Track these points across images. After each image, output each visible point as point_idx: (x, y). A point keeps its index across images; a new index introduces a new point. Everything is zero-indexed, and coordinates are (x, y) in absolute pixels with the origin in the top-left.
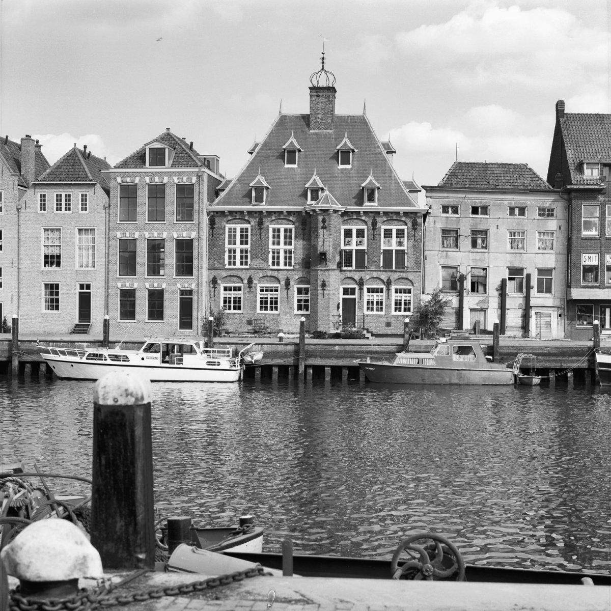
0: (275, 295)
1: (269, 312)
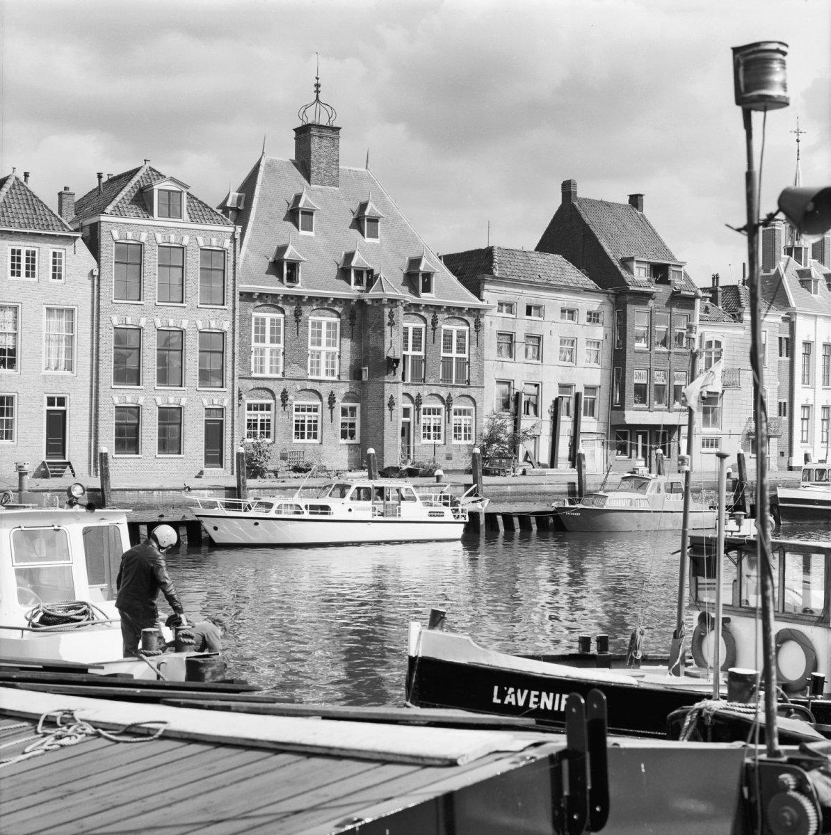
0: (254, 415)
1: (306, 441)
